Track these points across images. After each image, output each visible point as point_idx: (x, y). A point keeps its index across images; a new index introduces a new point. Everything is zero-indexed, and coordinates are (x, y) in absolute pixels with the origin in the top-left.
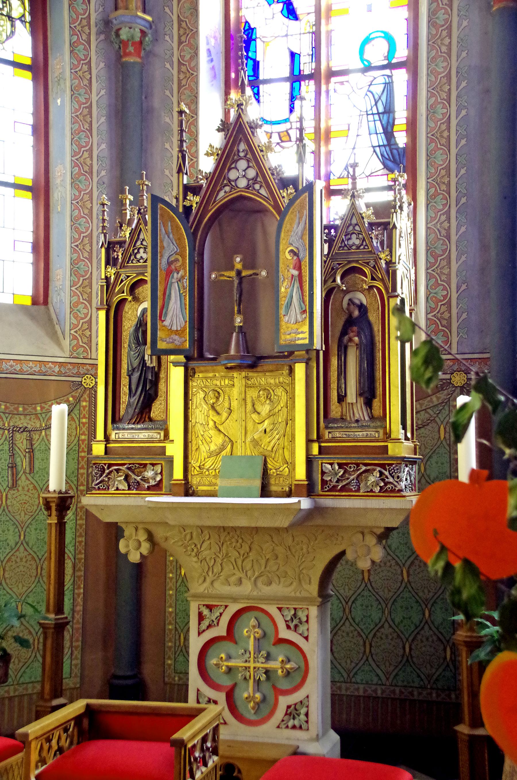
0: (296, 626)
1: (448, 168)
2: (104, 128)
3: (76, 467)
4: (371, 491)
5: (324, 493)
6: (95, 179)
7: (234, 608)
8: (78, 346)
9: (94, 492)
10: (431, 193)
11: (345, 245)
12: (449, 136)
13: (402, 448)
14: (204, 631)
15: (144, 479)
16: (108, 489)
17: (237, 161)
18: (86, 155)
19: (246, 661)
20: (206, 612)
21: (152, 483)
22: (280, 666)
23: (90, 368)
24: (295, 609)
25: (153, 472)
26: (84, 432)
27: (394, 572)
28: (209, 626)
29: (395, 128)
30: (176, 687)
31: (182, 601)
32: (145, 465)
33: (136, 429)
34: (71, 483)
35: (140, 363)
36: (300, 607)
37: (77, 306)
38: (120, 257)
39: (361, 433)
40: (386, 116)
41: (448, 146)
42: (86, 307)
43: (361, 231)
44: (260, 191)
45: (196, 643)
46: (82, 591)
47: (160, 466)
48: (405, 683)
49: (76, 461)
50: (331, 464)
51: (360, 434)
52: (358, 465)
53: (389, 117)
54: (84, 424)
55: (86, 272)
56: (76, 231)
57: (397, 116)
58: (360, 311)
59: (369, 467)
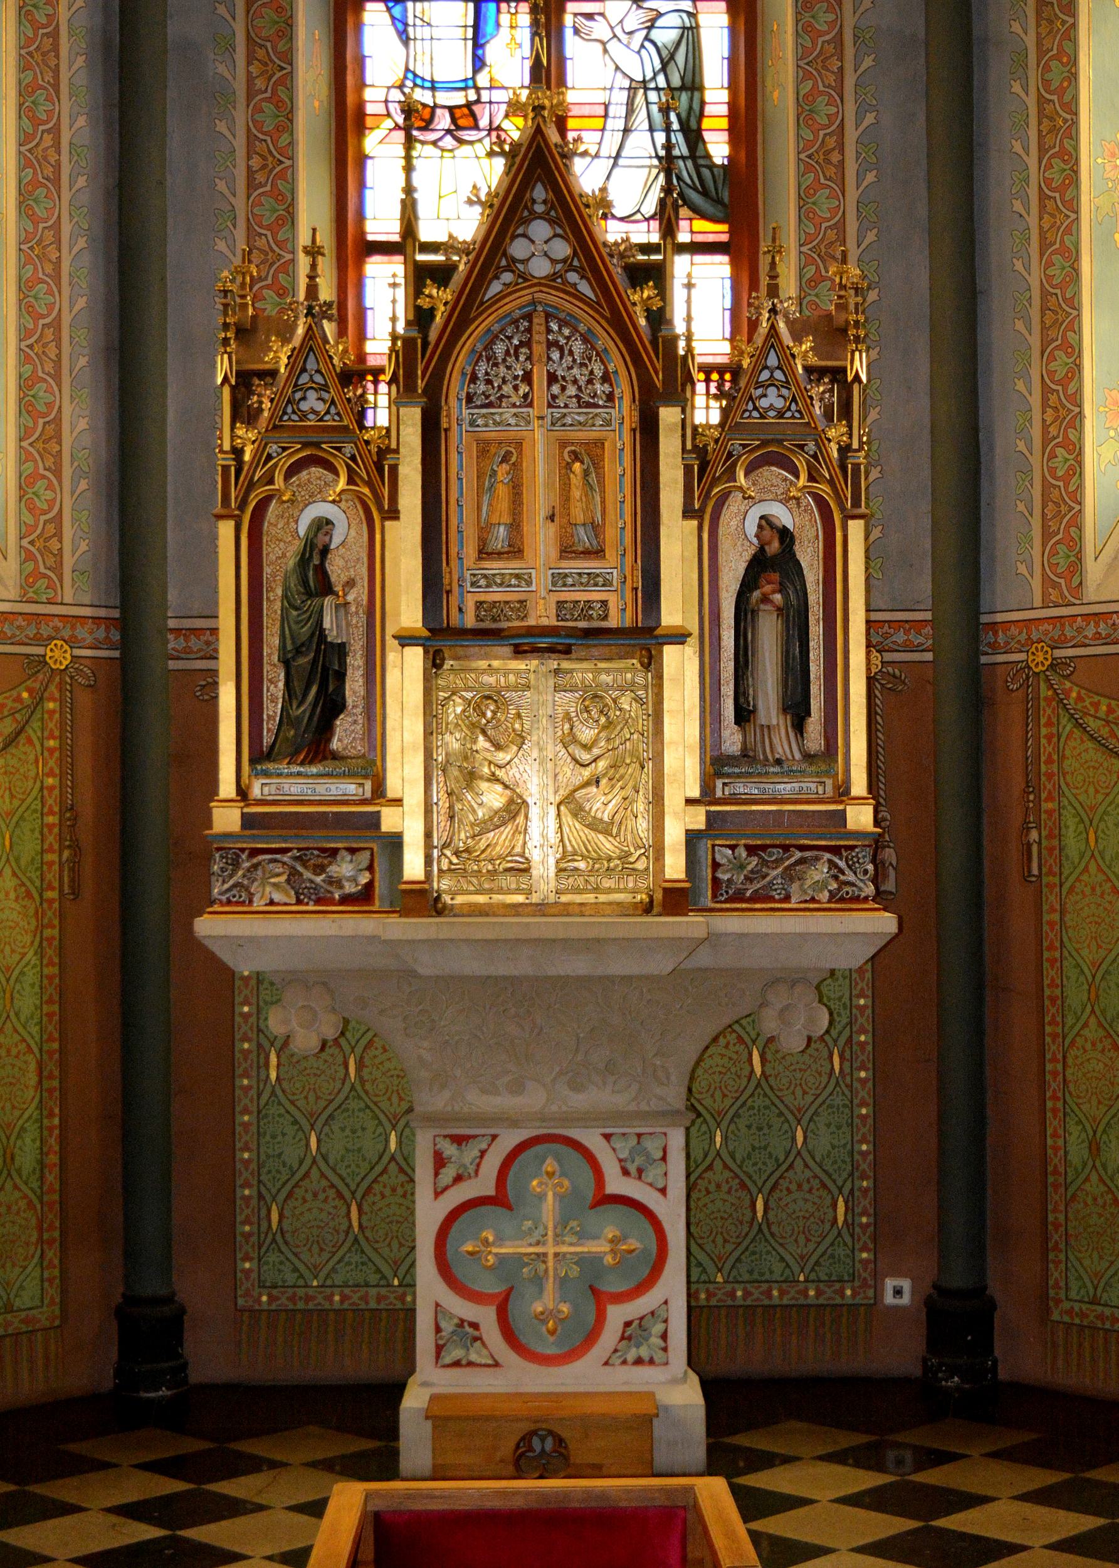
0: (640, 1171)
1: (840, 227)
2: (82, 80)
3: (39, 848)
4: (813, 900)
5: (718, 906)
6: (66, 195)
7: (510, 1139)
8: (36, 575)
9: (216, 908)
10: (808, 276)
11: (755, 408)
12: (842, 162)
13: (861, 817)
14: (446, 1188)
15: (338, 883)
16: (251, 902)
17: (526, 222)
18: (48, 140)
19: (538, 1243)
20: (449, 1149)
21: (350, 888)
22: (607, 1249)
23: (60, 625)
24: (639, 1135)
25: (351, 867)
26: (51, 769)
27: (735, 1057)
28: (458, 1179)
29: (706, 123)
30: (264, 1316)
31: (274, 1137)
32: (334, 852)
33: (307, 776)
34: (28, 884)
35: (313, 634)
36: (651, 1130)
37: (34, 483)
38: (267, 404)
39: (789, 786)
40: (684, 97)
41: (839, 182)
42: (50, 486)
43: (787, 382)
44: (579, 287)
45: (428, 1214)
46: (56, 1121)
47: (368, 853)
48: (756, 1276)
49: (37, 834)
50: (733, 848)
51: (786, 788)
52: (786, 848)
53: (691, 99)
54: (51, 751)
55: (49, 405)
56: (28, 313)
57: (709, 96)
58: (782, 542)
59: (808, 854)
